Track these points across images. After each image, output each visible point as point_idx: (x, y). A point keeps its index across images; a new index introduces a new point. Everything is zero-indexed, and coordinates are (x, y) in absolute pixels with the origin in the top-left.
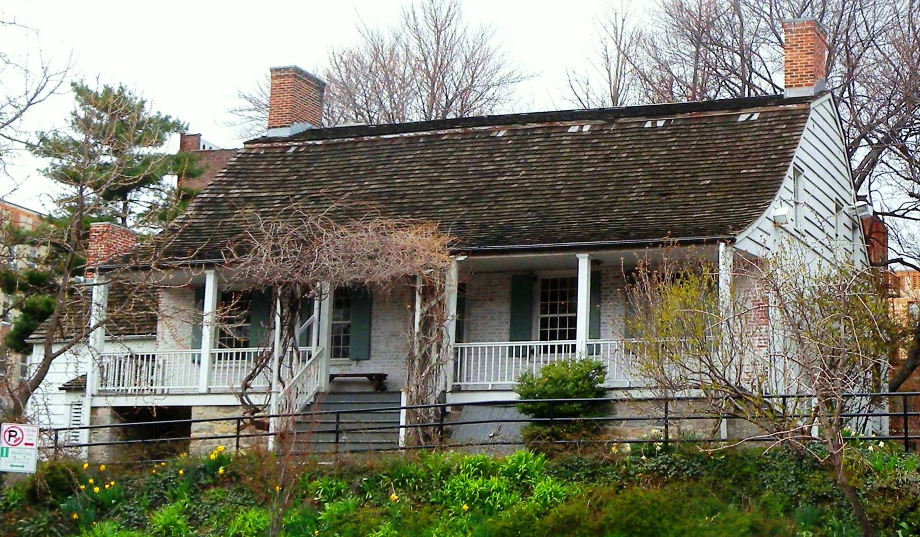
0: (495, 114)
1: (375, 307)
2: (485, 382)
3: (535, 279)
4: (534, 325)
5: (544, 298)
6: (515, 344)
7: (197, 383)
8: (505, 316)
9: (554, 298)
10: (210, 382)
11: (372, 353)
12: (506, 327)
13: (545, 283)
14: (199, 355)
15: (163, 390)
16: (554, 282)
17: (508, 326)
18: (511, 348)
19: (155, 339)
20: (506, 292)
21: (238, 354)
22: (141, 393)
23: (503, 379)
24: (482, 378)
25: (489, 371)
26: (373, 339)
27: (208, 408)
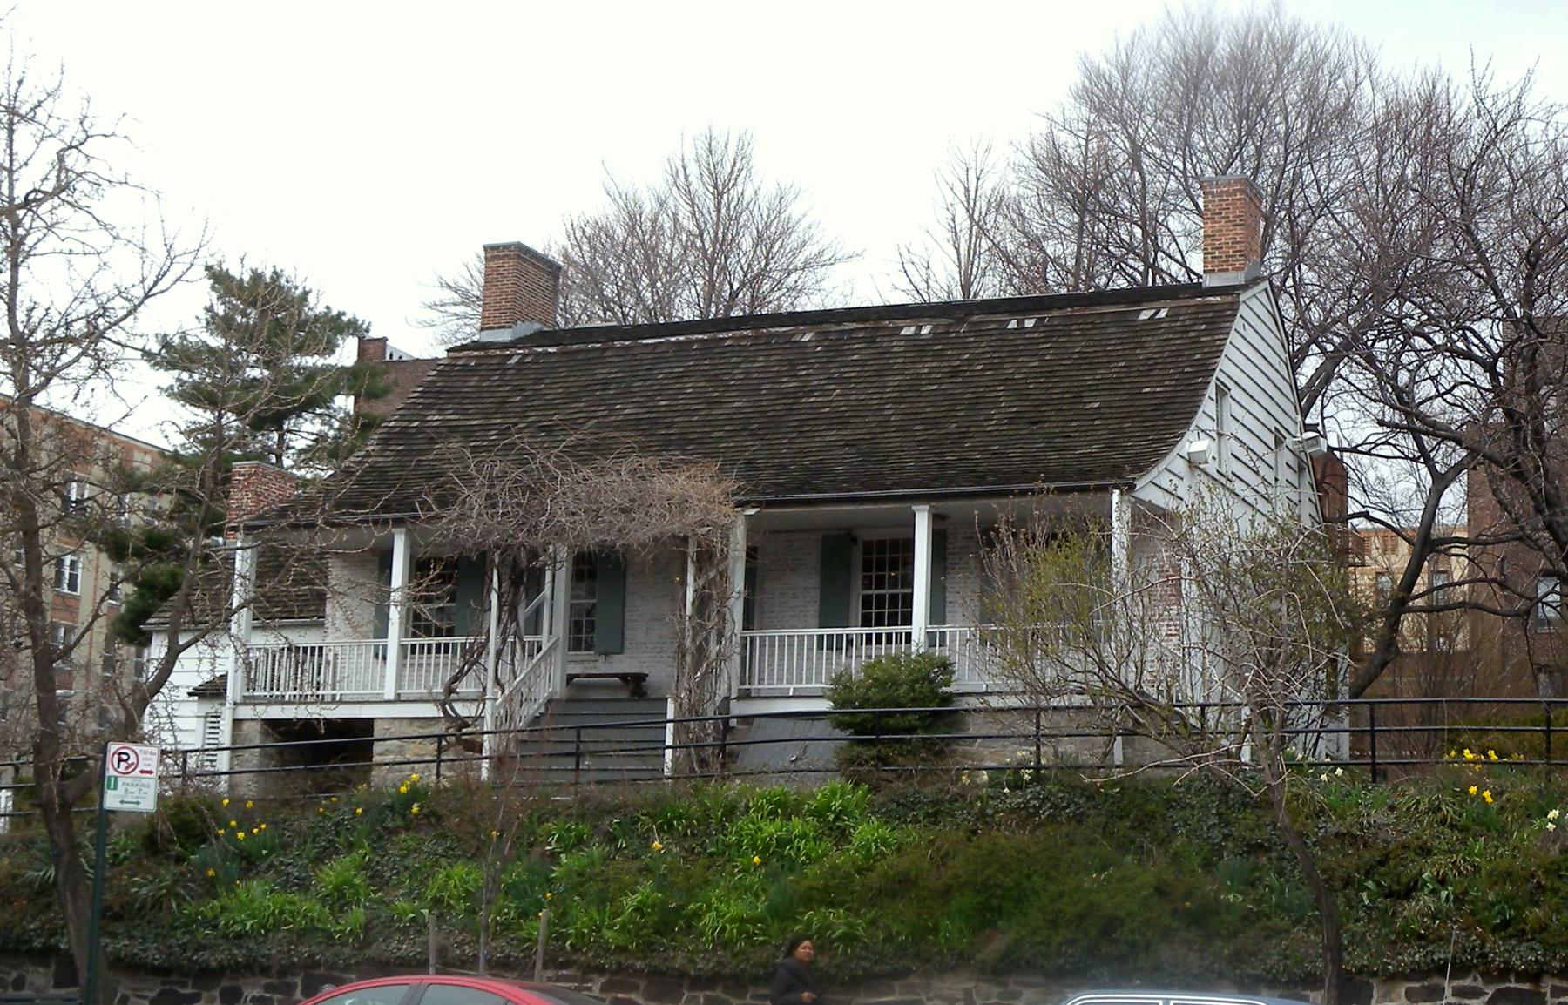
1: (630, 580)
3: (855, 540)
5: (867, 567)
6: (826, 631)
7: (382, 687)
9: (881, 567)
10: (399, 685)
11: (627, 644)
13: (868, 546)
14: (385, 647)
16: (881, 544)
18: (821, 637)
20: (814, 559)
22: (303, 701)
26: (628, 625)
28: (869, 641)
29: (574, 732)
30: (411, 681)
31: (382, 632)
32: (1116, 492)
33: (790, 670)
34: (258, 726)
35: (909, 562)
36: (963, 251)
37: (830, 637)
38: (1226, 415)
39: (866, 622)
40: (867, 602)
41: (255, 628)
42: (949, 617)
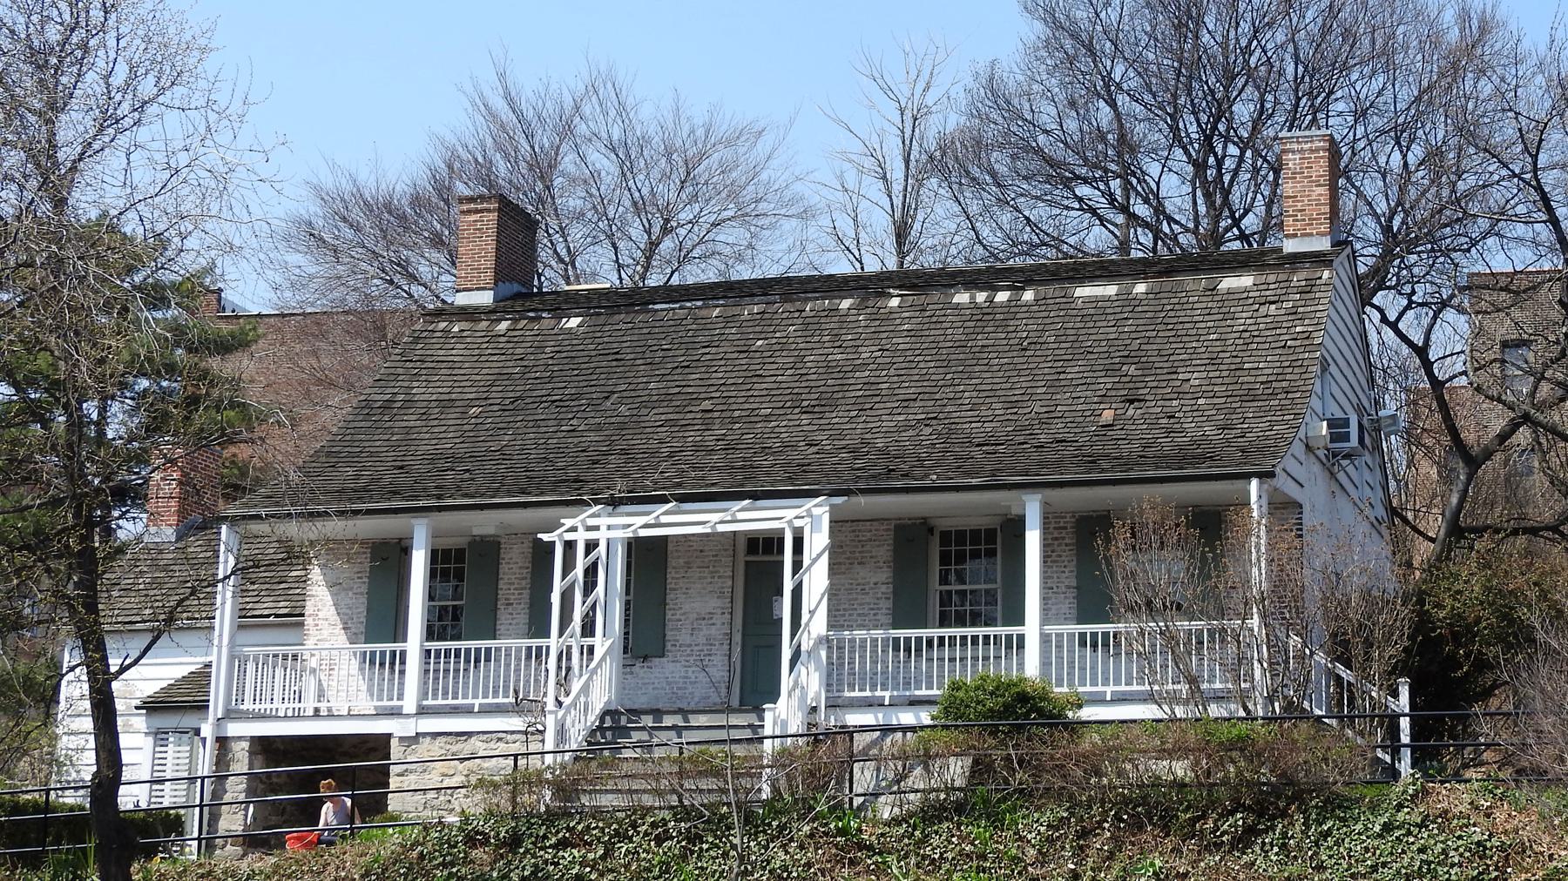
0: (491, 264)
1: (671, 574)
2: (1100, 688)
3: (931, 530)
4: (930, 602)
5: (945, 559)
6: (1088, 628)
7: (400, 697)
8: (883, 588)
9: (961, 558)
10: (424, 695)
11: (669, 645)
12: (886, 605)
13: (945, 537)
14: (403, 653)
15: (329, 710)
16: (961, 535)
17: (889, 604)
18: (529, 649)
19: (302, 624)
20: (884, 552)
21: (941, 639)
22: (298, 716)
23: (435, 696)
24: (445, 694)
25: (466, 684)
26: (670, 625)
27: (442, 739)
28: (1083, 643)
29: (511, 761)
30: (435, 690)
31: (397, 631)
32: (1254, 483)
33: (1083, 669)
34: (246, 745)
35: (781, 551)
36: (898, 202)
37: (908, 640)
38: (1327, 394)
39: (943, 623)
40: (945, 599)
41: (241, 627)
42: (501, 628)
